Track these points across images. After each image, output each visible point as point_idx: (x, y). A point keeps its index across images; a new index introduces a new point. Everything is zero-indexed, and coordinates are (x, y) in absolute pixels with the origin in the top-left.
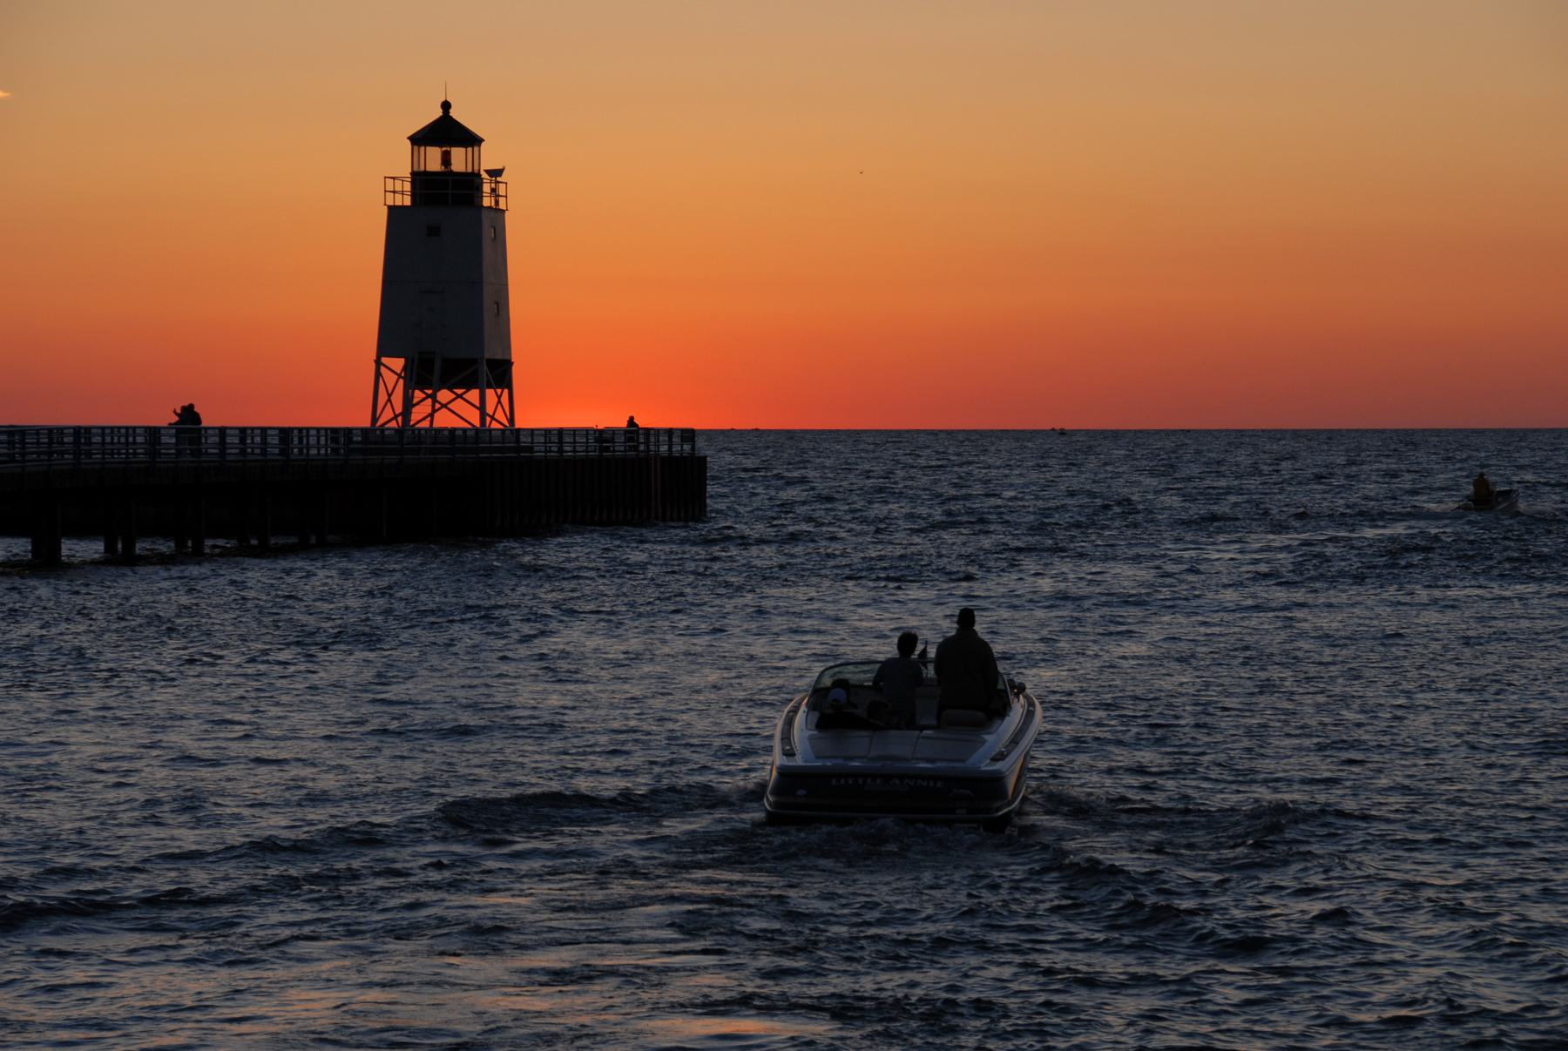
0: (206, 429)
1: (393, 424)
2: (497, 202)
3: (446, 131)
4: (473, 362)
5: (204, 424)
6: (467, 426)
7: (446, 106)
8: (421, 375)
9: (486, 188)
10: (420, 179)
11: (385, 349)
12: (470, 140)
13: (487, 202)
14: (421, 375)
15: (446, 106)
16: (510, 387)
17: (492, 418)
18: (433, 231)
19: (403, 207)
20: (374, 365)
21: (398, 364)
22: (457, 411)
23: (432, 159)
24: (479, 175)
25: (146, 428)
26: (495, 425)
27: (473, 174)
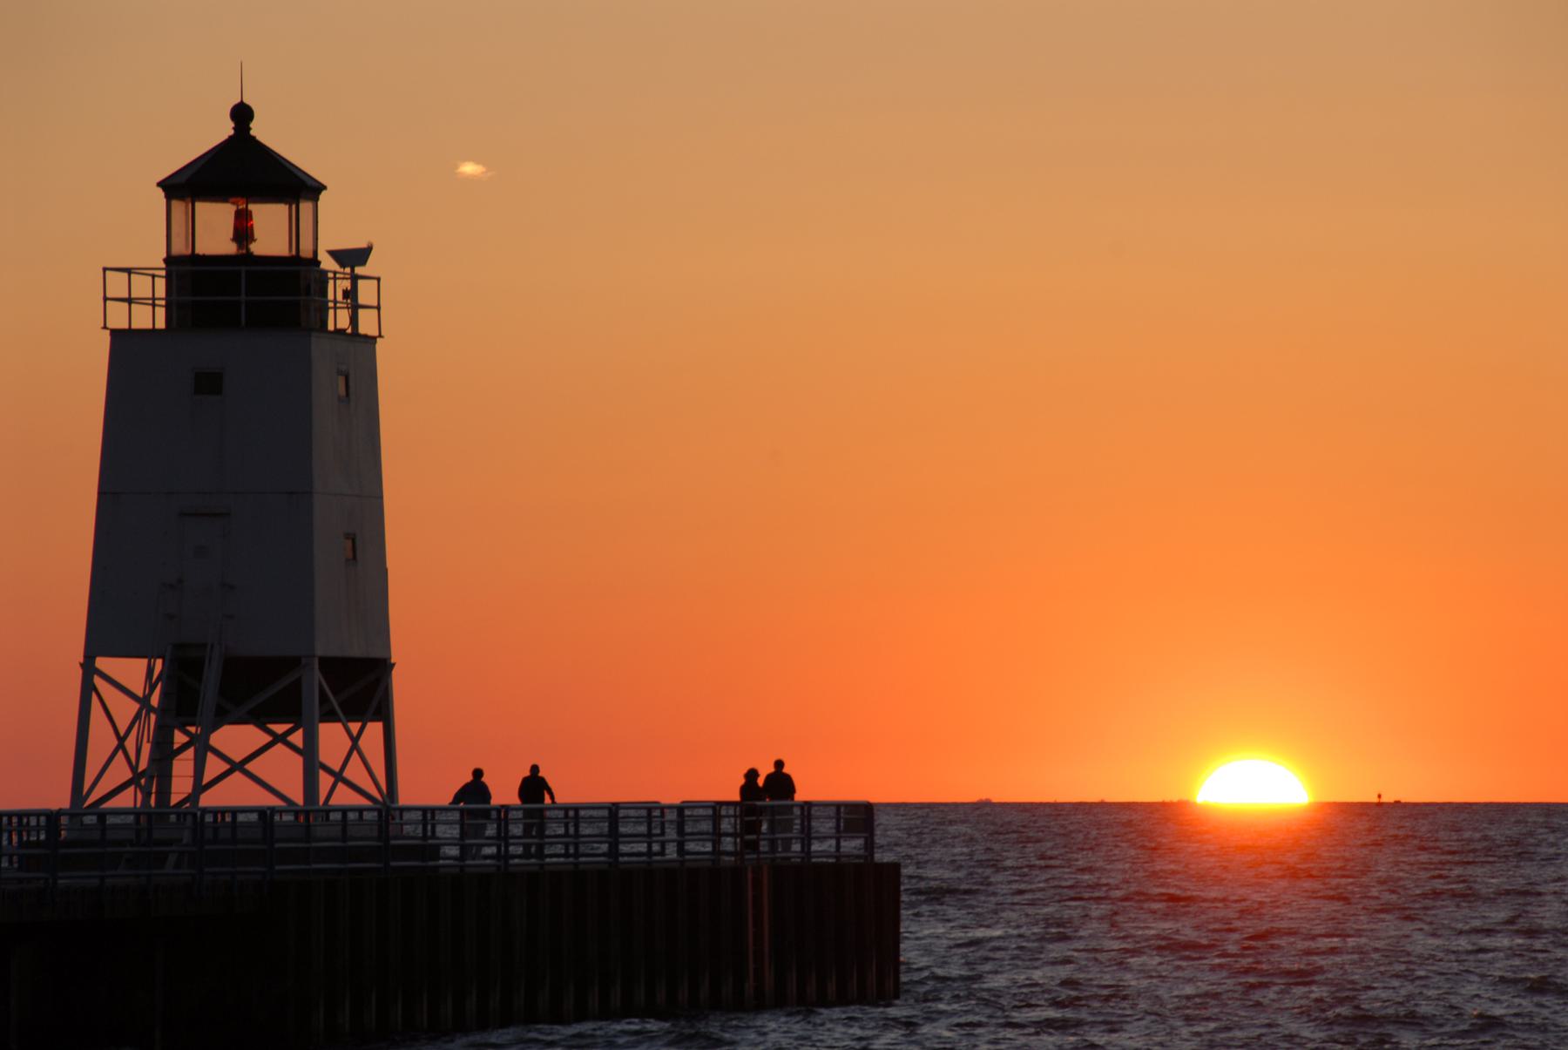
0: (402, 810)
1: (126, 800)
2: (354, 320)
3: (241, 168)
4: (294, 663)
5: (799, 797)
6: (271, 801)
7: (242, 114)
8: (205, 686)
9: (336, 290)
10: (189, 275)
11: (107, 632)
12: (296, 188)
13: (339, 319)
14: (205, 686)
15: (242, 114)
16: (383, 713)
17: (338, 777)
18: (209, 383)
19: (153, 331)
20: (79, 672)
21: (132, 671)
22: (251, 770)
23: (214, 227)
24: (315, 261)
25: (838, 806)
26: (344, 797)
27: (295, 260)
